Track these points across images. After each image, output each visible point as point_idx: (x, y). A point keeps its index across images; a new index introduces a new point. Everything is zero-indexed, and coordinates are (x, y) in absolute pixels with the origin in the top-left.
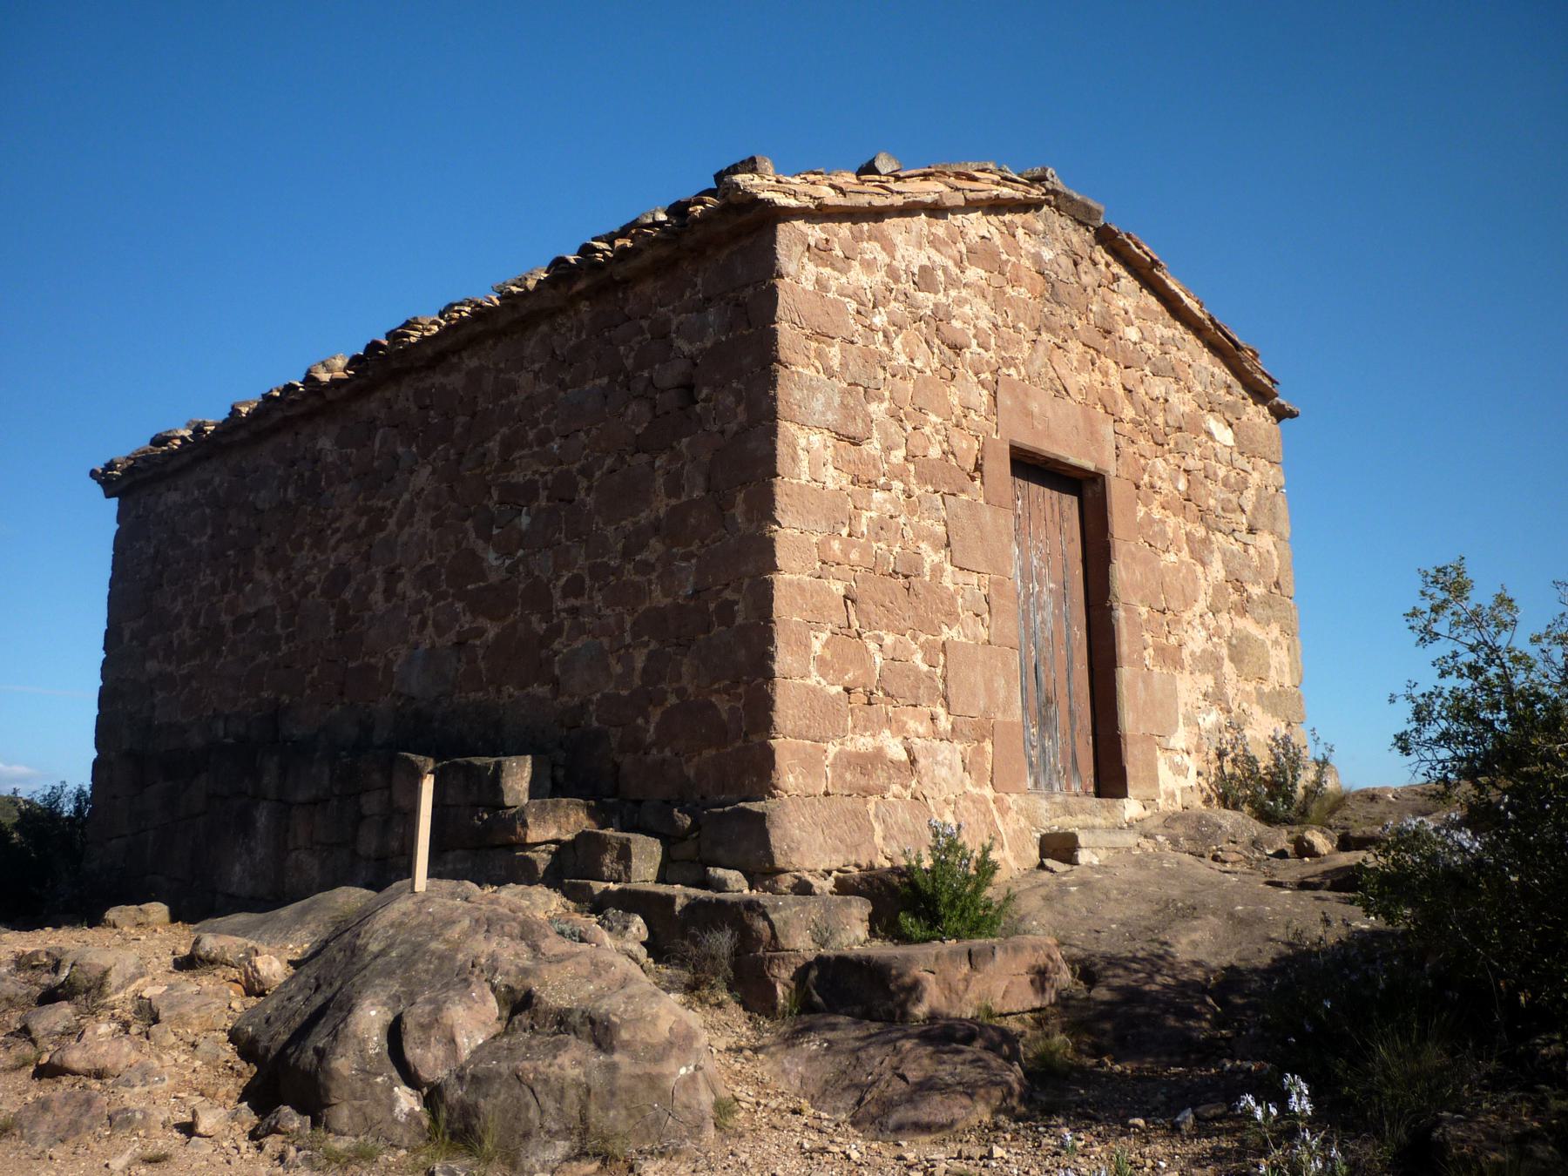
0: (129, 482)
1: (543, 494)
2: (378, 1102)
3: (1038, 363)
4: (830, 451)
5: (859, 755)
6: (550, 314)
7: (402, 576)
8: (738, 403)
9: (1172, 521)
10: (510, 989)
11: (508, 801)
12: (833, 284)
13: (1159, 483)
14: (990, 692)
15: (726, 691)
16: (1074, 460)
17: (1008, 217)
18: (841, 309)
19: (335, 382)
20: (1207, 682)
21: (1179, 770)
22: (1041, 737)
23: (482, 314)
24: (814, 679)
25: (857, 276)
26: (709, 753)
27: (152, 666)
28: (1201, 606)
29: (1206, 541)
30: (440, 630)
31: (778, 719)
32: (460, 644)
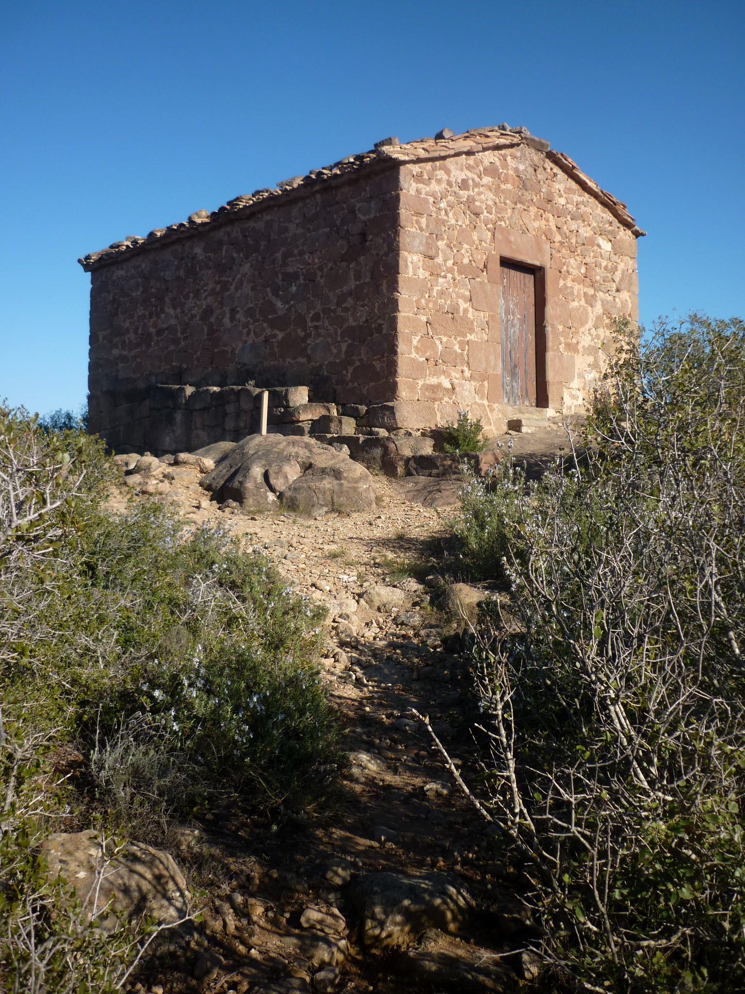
0: (103, 268)
1: (302, 278)
2: (262, 497)
3: (514, 219)
4: (421, 263)
5: (432, 386)
6: (303, 199)
7: (238, 312)
8: (384, 243)
9: (577, 287)
10: (304, 463)
11: (291, 405)
12: (424, 191)
13: (571, 270)
14: (488, 361)
15: (379, 359)
16: (530, 261)
17: (503, 152)
18: (426, 201)
19: (203, 224)
20: (591, 359)
21: (574, 397)
22: (511, 381)
23: (272, 198)
24: (414, 355)
25: (434, 187)
26: (372, 384)
27: (115, 352)
28: (590, 324)
29: (594, 296)
30: (257, 335)
31: (399, 370)
32: (266, 341)
